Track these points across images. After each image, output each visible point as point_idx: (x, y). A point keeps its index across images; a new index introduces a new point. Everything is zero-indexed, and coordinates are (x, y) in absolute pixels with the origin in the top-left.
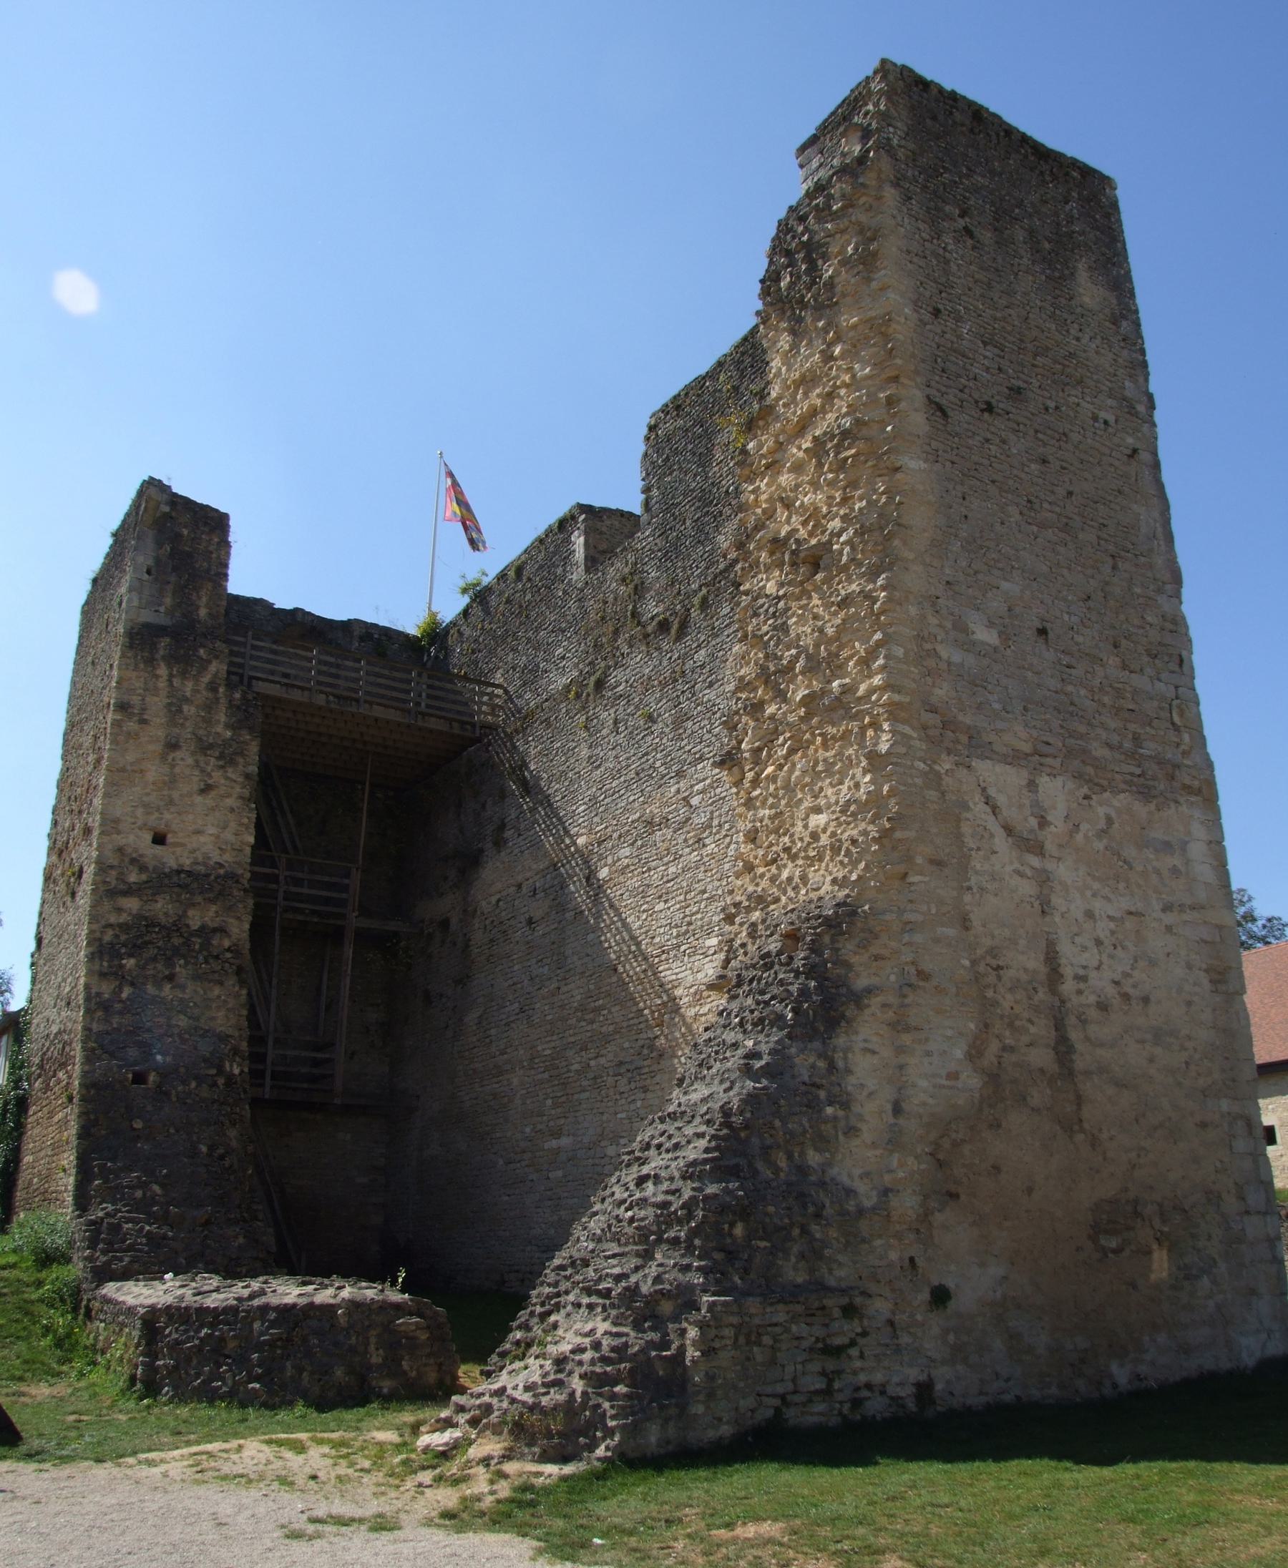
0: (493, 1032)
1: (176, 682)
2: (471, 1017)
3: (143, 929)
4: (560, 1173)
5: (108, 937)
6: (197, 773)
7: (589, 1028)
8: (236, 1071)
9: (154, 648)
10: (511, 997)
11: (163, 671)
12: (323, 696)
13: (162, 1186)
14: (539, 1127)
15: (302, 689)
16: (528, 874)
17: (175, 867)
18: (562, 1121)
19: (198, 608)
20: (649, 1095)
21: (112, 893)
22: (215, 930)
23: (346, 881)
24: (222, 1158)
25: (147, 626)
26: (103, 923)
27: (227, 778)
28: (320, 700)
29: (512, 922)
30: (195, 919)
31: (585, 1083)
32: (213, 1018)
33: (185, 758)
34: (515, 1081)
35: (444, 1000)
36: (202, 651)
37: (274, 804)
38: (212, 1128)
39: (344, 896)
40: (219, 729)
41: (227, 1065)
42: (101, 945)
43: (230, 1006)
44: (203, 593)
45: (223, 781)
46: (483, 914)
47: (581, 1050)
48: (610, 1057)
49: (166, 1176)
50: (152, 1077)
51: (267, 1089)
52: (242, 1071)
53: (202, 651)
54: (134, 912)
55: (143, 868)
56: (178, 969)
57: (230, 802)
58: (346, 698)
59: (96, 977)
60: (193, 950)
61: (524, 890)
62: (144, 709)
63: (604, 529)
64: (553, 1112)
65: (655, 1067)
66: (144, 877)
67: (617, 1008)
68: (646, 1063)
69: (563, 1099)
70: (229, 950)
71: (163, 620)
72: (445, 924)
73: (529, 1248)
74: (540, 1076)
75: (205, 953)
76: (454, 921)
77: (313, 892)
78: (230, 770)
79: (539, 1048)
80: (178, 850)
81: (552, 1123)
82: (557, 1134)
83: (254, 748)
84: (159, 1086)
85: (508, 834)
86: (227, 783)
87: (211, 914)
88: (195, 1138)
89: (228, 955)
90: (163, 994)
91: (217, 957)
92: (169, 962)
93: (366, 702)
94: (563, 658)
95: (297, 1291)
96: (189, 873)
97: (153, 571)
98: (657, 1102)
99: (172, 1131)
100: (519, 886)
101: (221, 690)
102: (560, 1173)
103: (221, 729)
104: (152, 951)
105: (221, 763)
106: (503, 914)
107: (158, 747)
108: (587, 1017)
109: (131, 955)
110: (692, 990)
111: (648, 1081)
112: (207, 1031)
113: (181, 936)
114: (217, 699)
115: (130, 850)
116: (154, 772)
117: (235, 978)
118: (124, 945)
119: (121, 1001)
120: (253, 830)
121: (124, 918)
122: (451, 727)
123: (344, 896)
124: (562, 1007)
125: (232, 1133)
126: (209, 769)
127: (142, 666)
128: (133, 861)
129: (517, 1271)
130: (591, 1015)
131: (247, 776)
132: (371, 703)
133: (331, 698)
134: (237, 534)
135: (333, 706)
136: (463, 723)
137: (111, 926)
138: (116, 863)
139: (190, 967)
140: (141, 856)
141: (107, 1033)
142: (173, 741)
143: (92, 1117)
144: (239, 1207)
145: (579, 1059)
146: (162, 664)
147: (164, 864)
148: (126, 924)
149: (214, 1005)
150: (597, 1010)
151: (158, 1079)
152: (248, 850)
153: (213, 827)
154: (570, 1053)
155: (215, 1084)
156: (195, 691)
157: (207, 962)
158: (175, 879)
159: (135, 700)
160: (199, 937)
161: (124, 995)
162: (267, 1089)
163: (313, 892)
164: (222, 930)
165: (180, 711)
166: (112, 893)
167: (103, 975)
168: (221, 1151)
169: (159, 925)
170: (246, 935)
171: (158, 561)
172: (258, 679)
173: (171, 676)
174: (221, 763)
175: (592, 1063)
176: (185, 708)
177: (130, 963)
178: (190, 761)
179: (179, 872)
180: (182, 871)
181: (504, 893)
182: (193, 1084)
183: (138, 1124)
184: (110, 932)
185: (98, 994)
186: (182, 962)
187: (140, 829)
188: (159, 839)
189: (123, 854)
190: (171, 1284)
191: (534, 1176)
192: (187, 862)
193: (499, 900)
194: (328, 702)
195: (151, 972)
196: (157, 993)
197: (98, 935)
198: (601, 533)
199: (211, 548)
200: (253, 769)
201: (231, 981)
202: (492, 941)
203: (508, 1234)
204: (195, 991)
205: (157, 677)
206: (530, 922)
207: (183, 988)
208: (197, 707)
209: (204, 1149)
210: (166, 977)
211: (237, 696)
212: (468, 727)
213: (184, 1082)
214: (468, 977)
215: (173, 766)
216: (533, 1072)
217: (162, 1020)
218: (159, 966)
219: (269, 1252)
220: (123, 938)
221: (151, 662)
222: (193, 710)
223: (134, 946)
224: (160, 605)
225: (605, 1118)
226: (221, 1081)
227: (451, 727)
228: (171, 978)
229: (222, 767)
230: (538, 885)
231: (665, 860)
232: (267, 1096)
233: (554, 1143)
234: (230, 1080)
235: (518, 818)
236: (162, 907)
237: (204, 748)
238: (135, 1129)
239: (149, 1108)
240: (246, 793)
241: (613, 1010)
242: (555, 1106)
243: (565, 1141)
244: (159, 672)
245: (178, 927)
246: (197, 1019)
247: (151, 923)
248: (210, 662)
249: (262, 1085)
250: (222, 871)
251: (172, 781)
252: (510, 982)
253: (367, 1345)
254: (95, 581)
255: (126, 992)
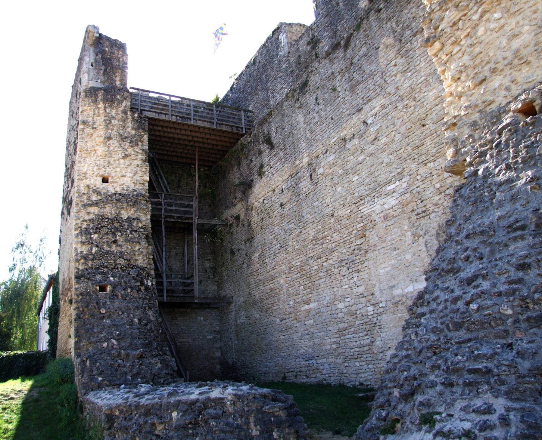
0: (267, 260)
1: (107, 110)
2: (255, 257)
3: (100, 220)
4: (312, 321)
5: (85, 226)
6: (120, 149)
7: (321, 247)
8: (150, 284)
9: (96, 96)
10: (275, 242)
11: (101, 105)
12: (175, 117)
13: (117, 340)
14: (297, 300)
15: (165, 114)
16: (278, 184)
17: (113, 192)
18: (310, 295)
19: (115, 81)
20: (361, 274)
21: (85, 206)
22: (134, 219)
23: (192, 203)
24: (146, 325)
25: (93, 88)
26: (82, 219)
27: (134, 151)
28: (174, 119)
29: (272, 208)
30: (125, 215)
31: (322, 275)
32: (136, 260)
33: (114, 143)
34: (282, 281)
35: (241, 251)
36: (118, 97)
37: (157, 173)
38: (140, 311)
39: (191, 209)
40: (129, 130)
41: (145, 281)
42: (81, 230)
43: (144, 253)
44: (117, 74)
45: (133, 153)
46: (256, 208)
47: (318, 259)
48: (335, 259)
49: (118, 335)
50: (109, 288)
51: (165, 298)
52: (152, 284)
53: (118, 97)
54: (96, 213)
55: (99, 193)
56: (118, 237)
57: (136, 162)
58: (185, 118)
59: (80, 244)
60: (125, 228)
61: (276, 191)
62: (94, 123)
63: (293, 31)
64: (305, 292)
65: (363, 258)
66: (99, 198)
67: (336, 234)
68: (357, 258)
69: (310, 284)
70: (142, 228)
71: (100, 85)
72: (238, 218)
73: (298, 360)
74: (295, 276)
75: (130, 229)
76: (242, 216)
77: (178, 208)
78: (136, 148)
79: (293, 263)
80: (115, 185)
81: (304, 298)
82: (308, 302)
83: (146, 138)
84: (112, 292)
85: (265, 169)
86: (135, 153)
87: (132, 212)
88: (132, 315)
89: (141, 230)
90: (112, 250)
91: (136, 231)
92: (114, 235)
93: (194, 119)
94: (282, 88)
95: (197, 392)
96: (120, 194)
97: (94, 64)
98: (367, 276)
99: (120, 313)
100: (274, 190)
101: (129, 113)
102: (312, 321)
103: (130, 129)
104: (105, 230)
105: (131, 145)
106: (267, 205)
107: (102, 139)
108: (318, 242)
109: (95, 233)
110: (382, 215)
111: (360, 267)
112: (134, 266)
113: (119, 222)
114: (127, 117)
115: (92, 186)
116: (101, 150)
117: (145, 240)
118: (92, 229)
119: (92, 254)
120: (148, 174)
121: (91, 216)
122: (232, 129)
123: (191, 209)
124: (304, 241)
125: (150, 313)
126: (126, 147)
127: (92, 104)
128: (94, 191)
129: (293, 372)
130: (321, 241)
131: (143, 150)
132: (196, 120)
133: (178, 118)
134: (129, 51)
135: (179, 121)
136: (237, 127)
137: (85, 220)
138: (86, 192)
139: (124, 236)
140: (98, 188)
141: (86, 269)
142: (108, 136)
143: (81, 309)
144: (156, 348)
145: (317, 264)
146: (101, 103)
147: (108, 191)
148: (92, 219)
149: (137, 253)
150: (324, 238)
151: (111, 288)
152: (147, 184)
153: (130, 173)
154: (311, 262)
155: (140, 290)
156: (117, 114)
157: (131, 233)
158: (114, 197)
159: (90, 119)
160: (127, 222)
161: (93, 251)
162: (165, 298)
163: (178, 208)
164: (138, 219)
165: (110, 122)
166: (85, 206)
167: (83, 243)
168: (145, 321)
169: (108, 218)
170: (149, 222)
171: (96, 61)
172: (145, 110)
173: (105, 107)
174: (131, 145)
175: (325, 264)
176: (113, 121)
177: (95, 236)
178: (117, 144)
179: (115, 194)
180: (116, 194)
181: (266, 196)
182: (129, 290)
183: (103, 311)
184: (85, 223)
185: (81, 252)
186: (120, 234)
187: (96, 176)
188: (105, 180)
189: (89, 188)
190: (122, 391)
191: (298, 325)
192: (118, 189)
193: (264, 200)
194: (177, 120)
195: (106, 240)
196: (109, 249)
197: (80, 225)
198: (293, 33)
199: (119, 56)
200: (146, 147)
201: (144, 242)
202: (262, 219)
203: (285, 354)
204: (127, 247)
205: (99, 108)
206: (281, 205)
207: (121, 246)
208: (118, 120)
209: (136, 320)
210: (113, 242)
211: (136, 115)
212: (240, 129)
213: (125, 290)
214: (252, 238)
215: (109, 147)
216: (291, 275)
217: (112, 261)
218: (110, 237)
219: (174, 371)
220: (91, 225)
221: (95, 102)
222: (116, 122)
223: (97, 228)
224: (98, 79)
225: (335, 290)
226: (143, 288)
227: (232, 129)
228: (115, 242)
229: (131, 146)
230: (283, 187)
231: (356, 154)
232: (165, 301)
233: (307, 307)
234: (147, 288)
235: (269, 160)
236: (109, 211)
237: (123, 138)
238: (102, 313)
239: (108, 303)
240: (144, 158)
241: (334, 235)
242: (305, 289)
243: (313, 305)
244: (100, 106)
245: (117, 218)
246: (129, 260)
247: (103, 218)
248: (122, 102)
249: (163, 296)
250: (135, 193)
251: (109, 154)
252: (274, 235)
253: (248, 423)
254: (72, 86)
255: (94, 250)
